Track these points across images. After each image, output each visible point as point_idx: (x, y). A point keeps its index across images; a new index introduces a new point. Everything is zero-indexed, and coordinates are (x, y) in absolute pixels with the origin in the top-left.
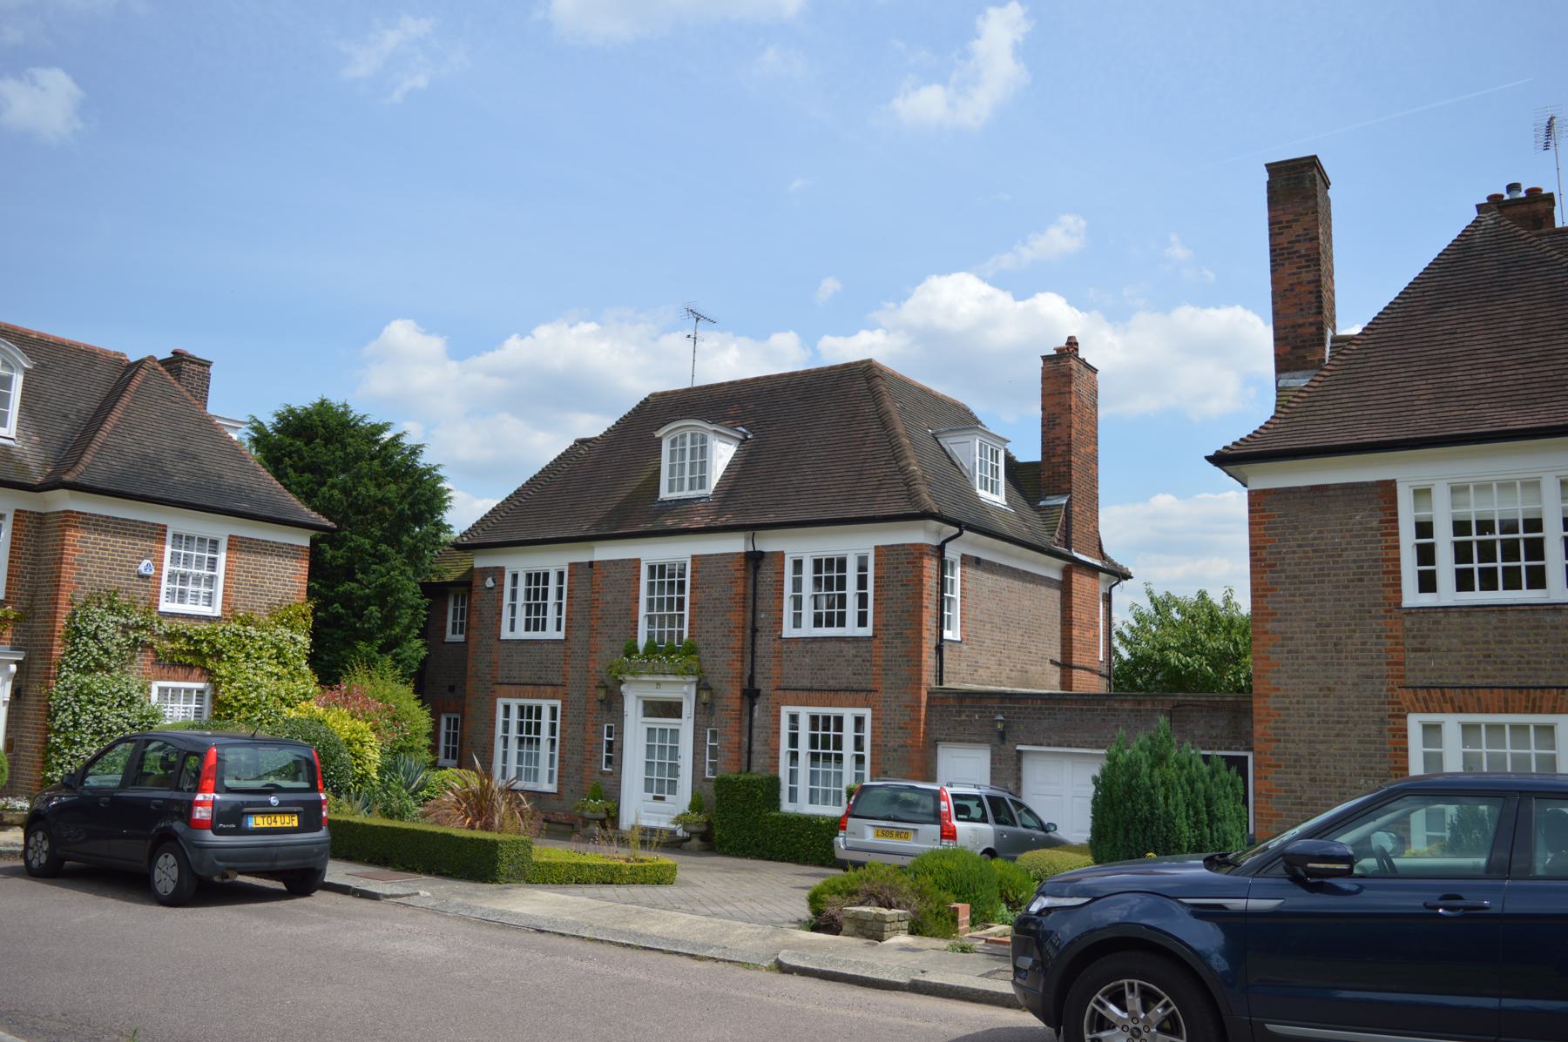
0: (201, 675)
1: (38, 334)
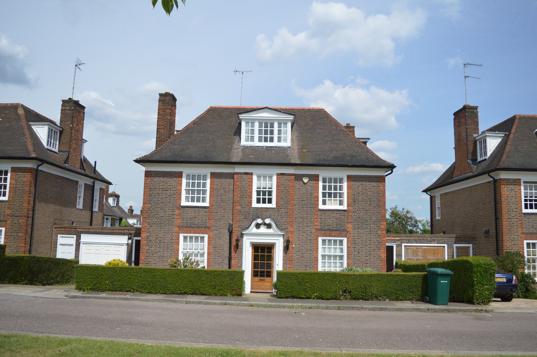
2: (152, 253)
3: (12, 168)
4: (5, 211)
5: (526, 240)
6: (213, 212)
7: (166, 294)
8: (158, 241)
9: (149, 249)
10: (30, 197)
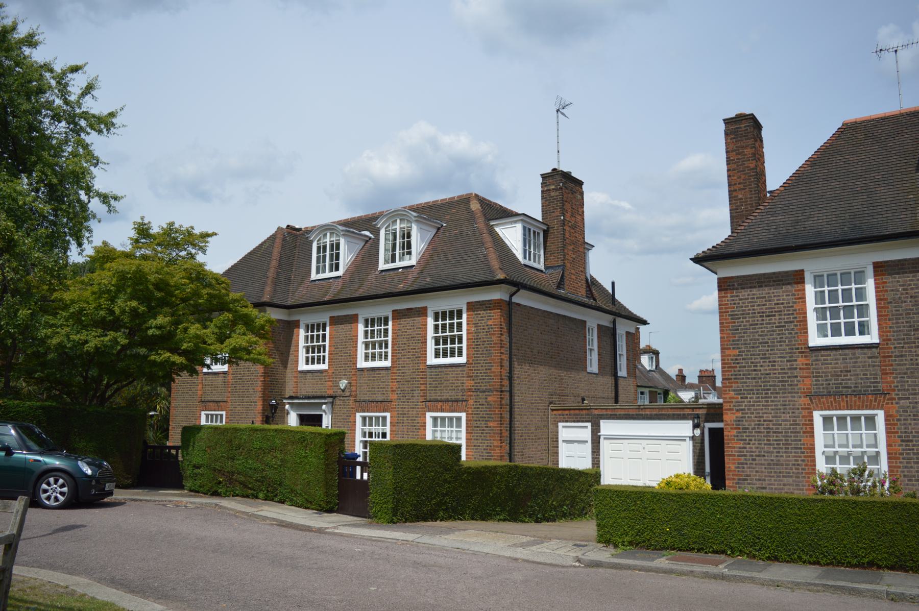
2: (752, 456)
3: (468, 303)
4: (463, 383)
6: (890, 356)
7: (817, 563)
8: (762, 430)
9: (745, 448)
10: (501, 353)
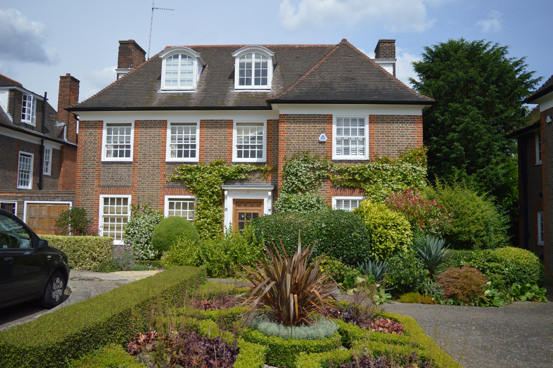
0: (360, 192)
1: (299, 45)
5: (102, 194)
